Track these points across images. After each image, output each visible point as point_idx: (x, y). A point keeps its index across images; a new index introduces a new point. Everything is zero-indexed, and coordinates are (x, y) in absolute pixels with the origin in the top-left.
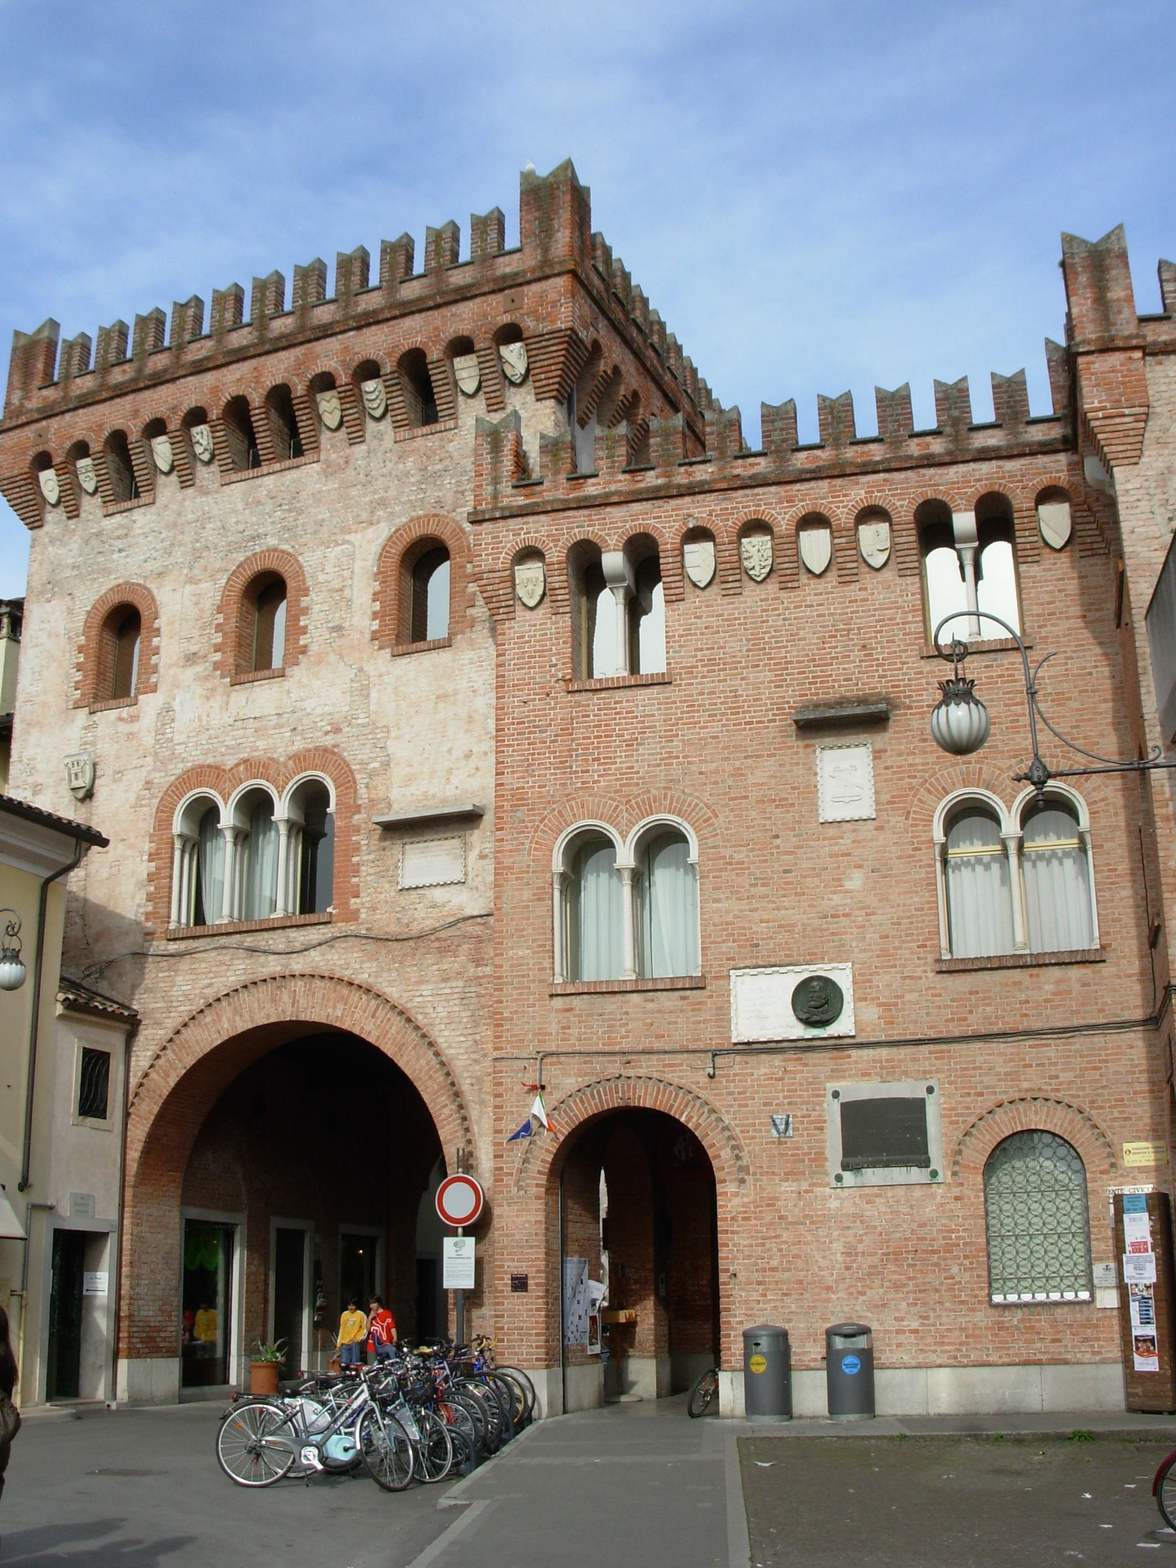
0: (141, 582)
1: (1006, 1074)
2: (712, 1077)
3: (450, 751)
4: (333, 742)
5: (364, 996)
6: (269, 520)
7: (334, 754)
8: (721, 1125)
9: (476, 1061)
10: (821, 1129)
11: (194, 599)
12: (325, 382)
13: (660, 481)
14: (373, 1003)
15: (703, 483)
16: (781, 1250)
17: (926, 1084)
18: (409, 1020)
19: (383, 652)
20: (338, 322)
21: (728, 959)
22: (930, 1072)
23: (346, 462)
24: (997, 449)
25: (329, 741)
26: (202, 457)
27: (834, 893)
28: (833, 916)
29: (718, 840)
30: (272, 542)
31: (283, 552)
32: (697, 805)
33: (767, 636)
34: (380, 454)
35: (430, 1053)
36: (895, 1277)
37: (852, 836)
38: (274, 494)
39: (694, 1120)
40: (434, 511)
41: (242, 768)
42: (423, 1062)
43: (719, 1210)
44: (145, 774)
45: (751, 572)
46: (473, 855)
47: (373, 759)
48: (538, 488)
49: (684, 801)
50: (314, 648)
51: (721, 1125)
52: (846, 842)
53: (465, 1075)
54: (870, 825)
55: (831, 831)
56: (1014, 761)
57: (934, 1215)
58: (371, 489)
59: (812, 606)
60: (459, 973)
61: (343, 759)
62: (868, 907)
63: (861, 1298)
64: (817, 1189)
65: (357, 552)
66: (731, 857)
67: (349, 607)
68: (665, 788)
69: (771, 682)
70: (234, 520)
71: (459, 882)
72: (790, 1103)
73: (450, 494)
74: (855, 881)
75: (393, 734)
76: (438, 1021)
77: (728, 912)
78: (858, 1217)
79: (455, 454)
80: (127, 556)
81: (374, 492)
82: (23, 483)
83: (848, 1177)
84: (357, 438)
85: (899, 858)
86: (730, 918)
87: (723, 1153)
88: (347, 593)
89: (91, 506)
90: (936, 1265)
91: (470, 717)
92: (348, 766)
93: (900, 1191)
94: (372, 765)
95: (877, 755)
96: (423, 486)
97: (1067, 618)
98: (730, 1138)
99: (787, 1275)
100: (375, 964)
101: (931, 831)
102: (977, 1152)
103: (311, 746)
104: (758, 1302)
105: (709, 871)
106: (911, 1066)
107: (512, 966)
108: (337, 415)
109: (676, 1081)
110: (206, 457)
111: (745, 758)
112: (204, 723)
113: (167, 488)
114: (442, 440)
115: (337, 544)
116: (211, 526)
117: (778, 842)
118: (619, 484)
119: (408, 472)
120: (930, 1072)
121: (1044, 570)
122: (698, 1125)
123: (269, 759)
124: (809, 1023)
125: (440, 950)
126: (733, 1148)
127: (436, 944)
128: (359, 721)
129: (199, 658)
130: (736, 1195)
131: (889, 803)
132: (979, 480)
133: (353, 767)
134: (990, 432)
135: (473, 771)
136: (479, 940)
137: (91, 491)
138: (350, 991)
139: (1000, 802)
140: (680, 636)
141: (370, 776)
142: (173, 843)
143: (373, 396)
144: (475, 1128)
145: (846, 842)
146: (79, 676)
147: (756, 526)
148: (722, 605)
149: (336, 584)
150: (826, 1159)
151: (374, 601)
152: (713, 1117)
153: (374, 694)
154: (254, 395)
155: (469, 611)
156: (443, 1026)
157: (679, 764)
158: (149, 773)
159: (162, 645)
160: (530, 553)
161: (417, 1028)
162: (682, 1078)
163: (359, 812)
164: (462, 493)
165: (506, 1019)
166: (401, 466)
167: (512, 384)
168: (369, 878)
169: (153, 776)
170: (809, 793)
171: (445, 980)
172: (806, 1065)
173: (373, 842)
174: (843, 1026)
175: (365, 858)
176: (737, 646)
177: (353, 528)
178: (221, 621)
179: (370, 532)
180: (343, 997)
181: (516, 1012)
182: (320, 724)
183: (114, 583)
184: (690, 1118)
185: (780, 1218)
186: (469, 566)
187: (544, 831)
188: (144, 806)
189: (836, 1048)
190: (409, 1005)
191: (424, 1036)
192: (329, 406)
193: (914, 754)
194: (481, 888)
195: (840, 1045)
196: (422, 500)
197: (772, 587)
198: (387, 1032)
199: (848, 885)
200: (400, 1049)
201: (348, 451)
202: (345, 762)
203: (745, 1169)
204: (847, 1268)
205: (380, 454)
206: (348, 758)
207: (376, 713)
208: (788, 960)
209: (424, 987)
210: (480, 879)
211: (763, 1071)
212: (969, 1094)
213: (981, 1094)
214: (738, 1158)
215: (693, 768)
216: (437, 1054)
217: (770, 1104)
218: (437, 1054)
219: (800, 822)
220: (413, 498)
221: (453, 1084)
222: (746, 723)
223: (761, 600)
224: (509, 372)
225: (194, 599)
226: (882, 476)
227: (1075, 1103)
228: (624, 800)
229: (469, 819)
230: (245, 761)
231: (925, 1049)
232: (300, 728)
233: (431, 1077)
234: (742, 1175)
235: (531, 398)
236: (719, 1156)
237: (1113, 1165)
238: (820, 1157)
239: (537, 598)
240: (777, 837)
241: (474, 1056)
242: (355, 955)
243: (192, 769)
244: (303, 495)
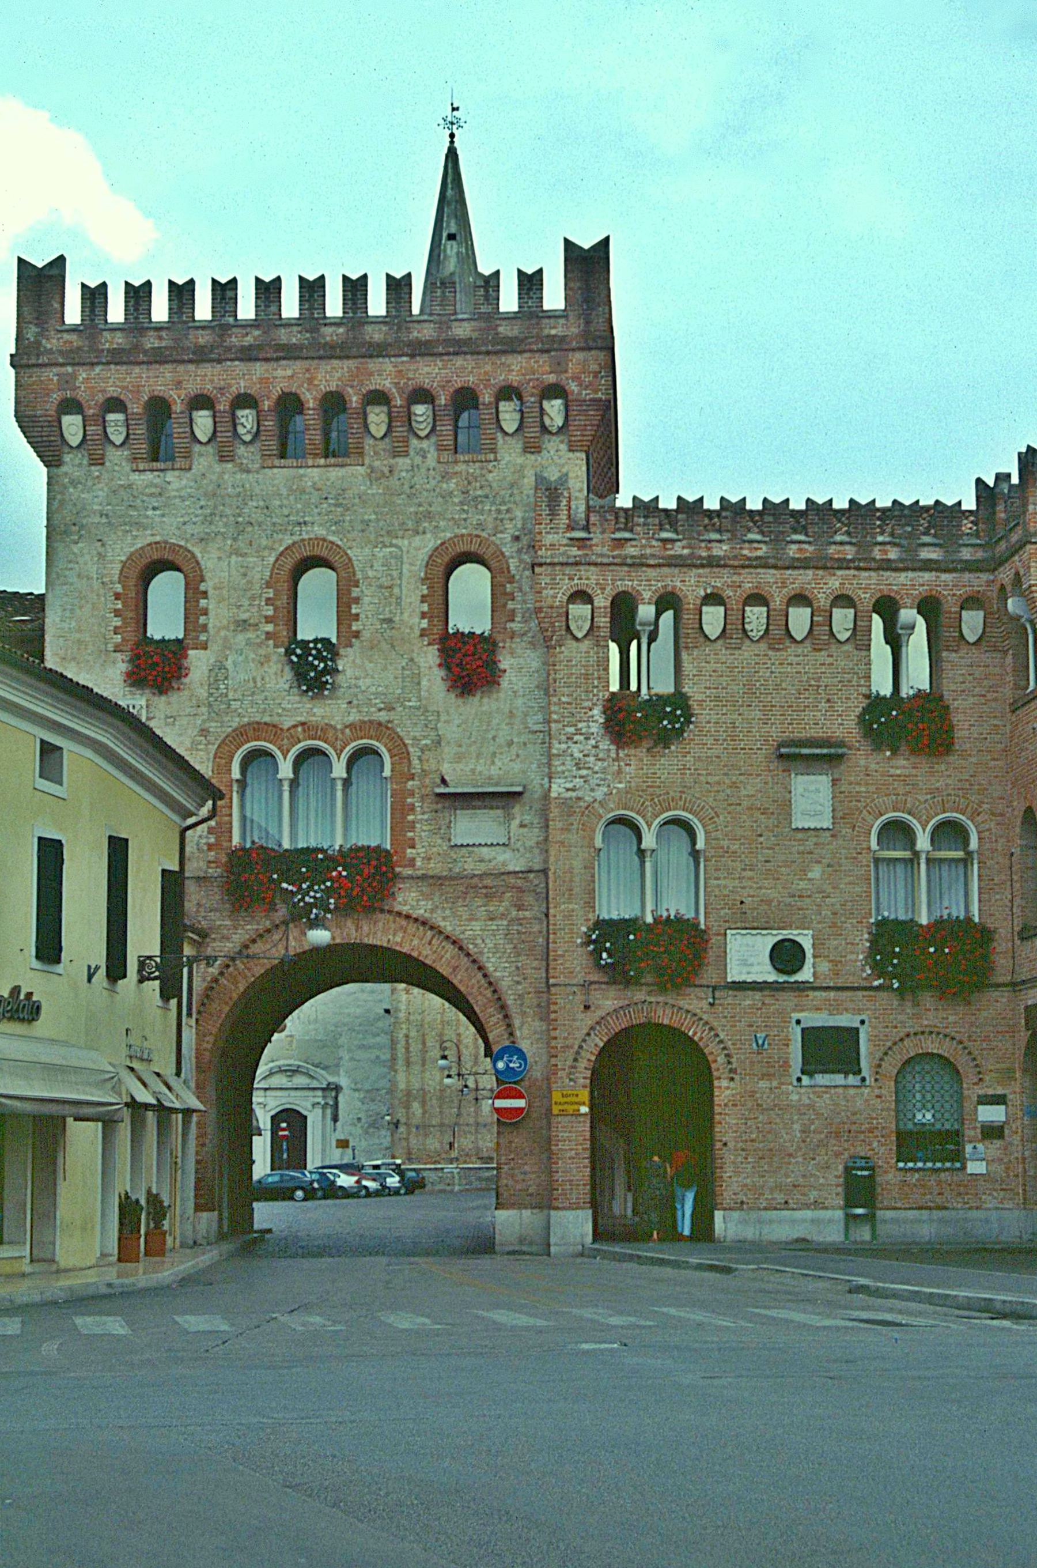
0: (182, 543)
1: (913, 1014)
2: (712, 1005)
3: (494, 738)
4: (387, 718)
5: (421, 928)
6: (316, 510)
7: (388, 728)
8: (717, 1039)
9: (518, 983)
10: (787, 1045)
11: (242, 570)
12: (378, 398)
13: (686, 551)
14: (429, 933)
15: (720, 558)
16: (758, 1128)
17: (860, 1018)
18: (461, 948)
19: (431, 647)
20: (390, 345)
21: (725, 922)
22: (863, 1010)
23: (390, 471)
24: (936, 561)
25: (383, 716)
26: (244, 437)
27: (801, 880)
28: (799, 896)
29: (719, 834)
30: (320, 531)
31: (332, 543)
32: (704, 807)
33: (758, 684)
34: (423, 470)
35: (480, 975)
36: (835, 1148)
37: (814, 840)
38: (319, 485)
39: (699, 1034)
40: (475, 532)
41: (300, 729)
42: (473, 981)
43: (716, 1099)
44: (199, 722)
45: (750, 634)
46: (515, 823)
47: (425, 737)
48: (588, 543)
49: (695, 802)
50: (366, 635)
51: (717, 1039)
52: (810, 844)
53: (510, 992)
54: (827, 834)
55: (800, 835)
56: (929, 797)
57: (863, 1107)
58: (416, 501)
59: (792, 664)
60: (503, 915)
61: (396, 733)
62: (824, 892)
63: (813, 1162)
64: (783, 1087)
65: (405, 557)
66: (728, 847)
67: (399, 604)
68: (681, 792)
69: (760, 719)
70: (278, 503)
71: (504, 844)
72: (766, 1026)
73: (490, 519)
74: (816, 872)
75: (443, 718)
76: (486, 950)
77: (725, 887)
78: (811, 1106)
79: (494, 485)
80: (163, 515)
81: (420, 505)
82: (46, 424)
83: (806, 1080)
84: (400, 451)
85: (846, 858)
86: (726, 892)
87: (719, 1059)
88: (396, 590)
89: (116, 457)
90: (864, 1141)
91: (511, 712)
92: (401, 740)
93: (840, 1090)
94: (424, 742)
95: (835, 782)
96: (466, 508)
97: (974, 696)
98: (724, 1048)
99: (761, 1145)
100: (430, 903)
101: (869, 841)
102: (891, 1067)
103: (366, 719)
104: (742, 1163)
105: (712, 857)
106: (851, 1006)
107: (564, 916)
108: (384, 428)
109: (686, 1007)
110: (248, 438)
111: (741, 774)
112: (259, 684)
113: (204, 460)
114: (482, 468)
115: (385, 546)
116: (255, 504)
117: (761, 839)
118: (653, 549)
119: (452, 492)
120: (863, 1010)
121: (960, 657)
122: (701, 1039)
123: (327, 724)
124: (780, 971)
125: (486, 896)
126: (727, 1055)
127: (484, 891)
128: (411, 704)
129: (250, 625)
130: (728, 1088)
131: (841, 818)
132: (923, 585)
133: (407, 742)
134: (931, 548)
135: (514, 757)
136: (520, 890)
137: (118, 443)
138: (408, 923)
139: (918, 825)
140: (694, 676)
141: (422, 751)
142: (231, 786)
143: (421, 419)
144: (518, 1033)
145: (810, 844)
146: (117, 622)
147: (757, 599)
148: (725, 655)
149: (385, 581)
150: (790, 1066)
151: (422, 602)
152: (712, 1033)
153: (424, 683)
154: (308, 396)
155: (509, 625)
156: (491, 955)
157: (691, 774)
158: (204, 721)
159: (210, 607)
160: (581, 596)
161: (468, 955)
162: (690, 1004)
163: (413, 779)
164: (502, 520)
165: (560, 956)
166: (445, 486)
167: (550, 433)
168: (423, 834)
169: (207, 725)
170: (786, 807)
171: (492, 919)
172: (777, 1000)
173: (425, 805)
174: (806, 975)
175: (419, 817)
176: (736, 688)
177: (400, 533)
178: (271, 595)
179: (417, 540)
180: (402, 927)
181: (566, 951)
182: (374, 701)
183: (150, 539)
184: (695, 1033)
185: (758, 1105)
186: (508, 586)
187: (588, 816)
188: (201, 750)
189: (798, 989)
190: (461, 936)
191: (474, 961)
192: (377, 419)
193: (860, 784)
194: (522, 850)
195: (802, 987)
196: (465, 520)
197: (763, 646)
198: (442, 957)
199: (810, 875)
200: (454, 970)
201: (392, 461)
202: (399, 736)
203: (733, 1071)
204: (804, 1141)
205: (423, 470)
206: (401, 734)
207: (426, 699)
208: (767, 925)
209: (474, 923)
210: (520, 843)
211: (748, 1002)
212: (887, 1027)
213: (896, 1027)
214: (729, 1063)
215: (702, 778)
216: (485, 976)
217: (752, 1026)
218: (485, 976)
219: (778, 827)
220: (457, 517)
221: (499, 999)
222: (742, 749)
223: (756, 655)
224: (547, 422)
225: (242, 570)
226: (852, 572)
227: (958, 1037)
228: (649, 798)
229: (512, 797)
230: (303, 724)
231: (860, 993)
232: (355, 702)
233: (481, 993)
234: (732, 1075)
235: (563, 447)
236: (715, 1061)
237: (981, 1080)
238: (786, 1064)
239: (585, 632)
240: (761, 835)
241: (516, 978)
242: (413, 894)
243: (249, 724)
244: (349, 494)
